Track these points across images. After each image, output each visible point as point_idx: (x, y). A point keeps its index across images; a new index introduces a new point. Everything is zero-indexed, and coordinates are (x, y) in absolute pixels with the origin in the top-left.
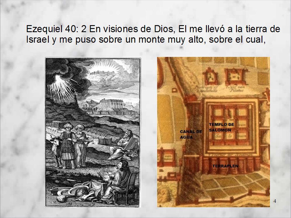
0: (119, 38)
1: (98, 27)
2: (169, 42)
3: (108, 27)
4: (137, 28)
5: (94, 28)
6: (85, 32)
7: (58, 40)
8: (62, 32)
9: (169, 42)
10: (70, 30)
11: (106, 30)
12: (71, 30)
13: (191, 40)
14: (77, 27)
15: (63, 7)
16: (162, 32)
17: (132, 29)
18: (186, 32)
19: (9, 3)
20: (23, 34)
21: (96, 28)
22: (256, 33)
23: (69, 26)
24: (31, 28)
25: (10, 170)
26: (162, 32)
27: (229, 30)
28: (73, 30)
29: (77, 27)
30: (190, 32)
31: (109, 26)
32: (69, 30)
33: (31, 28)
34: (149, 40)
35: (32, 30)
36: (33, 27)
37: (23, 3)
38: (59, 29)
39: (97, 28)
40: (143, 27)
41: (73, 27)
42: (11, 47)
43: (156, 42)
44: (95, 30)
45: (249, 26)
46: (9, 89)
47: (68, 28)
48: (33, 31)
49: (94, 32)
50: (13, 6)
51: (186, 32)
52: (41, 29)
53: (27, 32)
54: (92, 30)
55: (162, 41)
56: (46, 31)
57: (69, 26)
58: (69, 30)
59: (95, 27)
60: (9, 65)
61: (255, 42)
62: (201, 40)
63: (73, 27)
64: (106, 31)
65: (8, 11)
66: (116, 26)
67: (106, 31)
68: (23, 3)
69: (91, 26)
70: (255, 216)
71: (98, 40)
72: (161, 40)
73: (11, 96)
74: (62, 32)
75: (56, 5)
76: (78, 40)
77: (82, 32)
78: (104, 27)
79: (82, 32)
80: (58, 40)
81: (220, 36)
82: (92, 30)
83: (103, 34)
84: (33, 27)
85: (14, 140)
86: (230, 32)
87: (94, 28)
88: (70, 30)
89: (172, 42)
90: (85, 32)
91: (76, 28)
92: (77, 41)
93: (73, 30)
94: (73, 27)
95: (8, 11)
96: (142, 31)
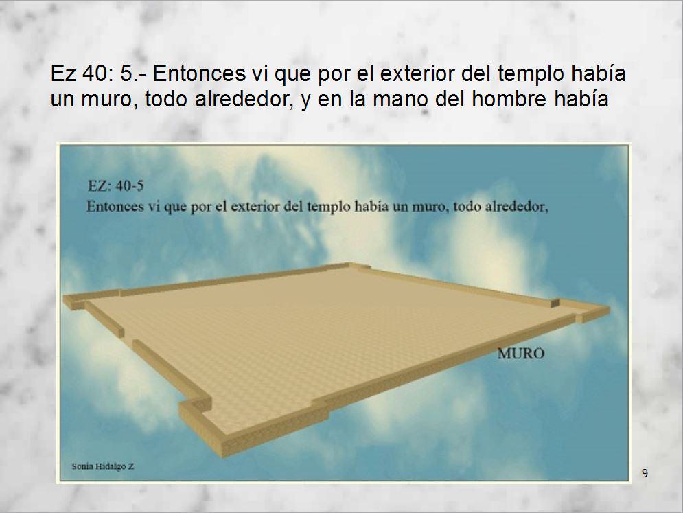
0: (538, 96)
1: (337, 95)
2: (83, 106)
3: (264, 68)
4: (244, 71)
5: (164, 72)
6: (75, 80)
7: (314, 102)
8: (488, 80)
9: (83, 106)
10: (93, 76)
11: (257, 76)
12: (95, 75)
13: (201, 101)
14: (111, 70)
15: (148, 18)
16: (550, 80)
17: (232, 74)
18: (170, 80)
19: (21, 8)
20: (46, 88)
21: (167, 72)
22: (596, 83)
23: (90, 66)
24: (62, 72)
25: (22, 401)
26: (594, 105)
27: (198, 101)
28: (101, 77)
29: (111, 70)
30: (375, 106)
31: (266, 66)
32: (91, 76)
33: (62, 72)
34: (490, 100)
35: (64, 76)
36: (68, 70)
37: (53, 9)
38: (366, 74)
39: (170, 71)
40: (467, 70)
41: (101, 69)
42: (26, 111)
43: (97, 106)
44: (166, 76)
45: (433, 68)
46: (19, 211)
47: (89, 70)
48: (68, 79)
49: (165, 80)
50: (30, 16)
51: (170, 80)
52: (254, 100)
53: (53, 80)
54: (159, 76)
55: (509, 77)
56: (284, 78)
57: (90, 66)
58: (91, 76)
59: (166, 69)
60: (20, 154)
61: (297, 80)
62: (126, 100)
63: (101, 68)
64: (257, 79)
65: (17, 26)
66: (266, 66)
67: (257, 79)
68: (53, 9)
69: (124, 66)
70: (597, 509)
71: (346, 99)
72: (413, 75)
73: (26, 225)
74: (462, 105)
75: (132, 11)
76: (324, 75)
77: (74, 70)
78: (253, 69)
79: (74, 70)
80: (314, 102)
81: (598, 66)
82: (159, 76)
83: (547, 88)
84: (68, 70)
85: (32, 330)
86: (572, 105)
87: (164, 72)
88: (93, 76)
89: (72, 106)
90: (75, 80)
91: (108, 70)
92: (321, 78)
93: (101, 77)
94: (101, 69)
95: (17, 26)
96: (438, 104)
